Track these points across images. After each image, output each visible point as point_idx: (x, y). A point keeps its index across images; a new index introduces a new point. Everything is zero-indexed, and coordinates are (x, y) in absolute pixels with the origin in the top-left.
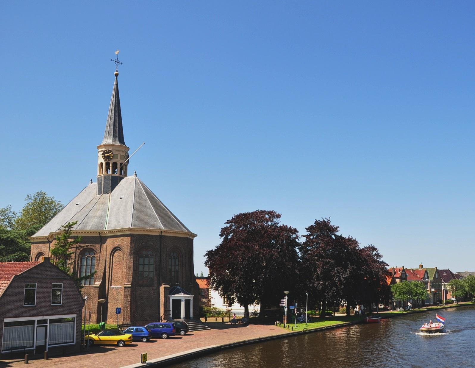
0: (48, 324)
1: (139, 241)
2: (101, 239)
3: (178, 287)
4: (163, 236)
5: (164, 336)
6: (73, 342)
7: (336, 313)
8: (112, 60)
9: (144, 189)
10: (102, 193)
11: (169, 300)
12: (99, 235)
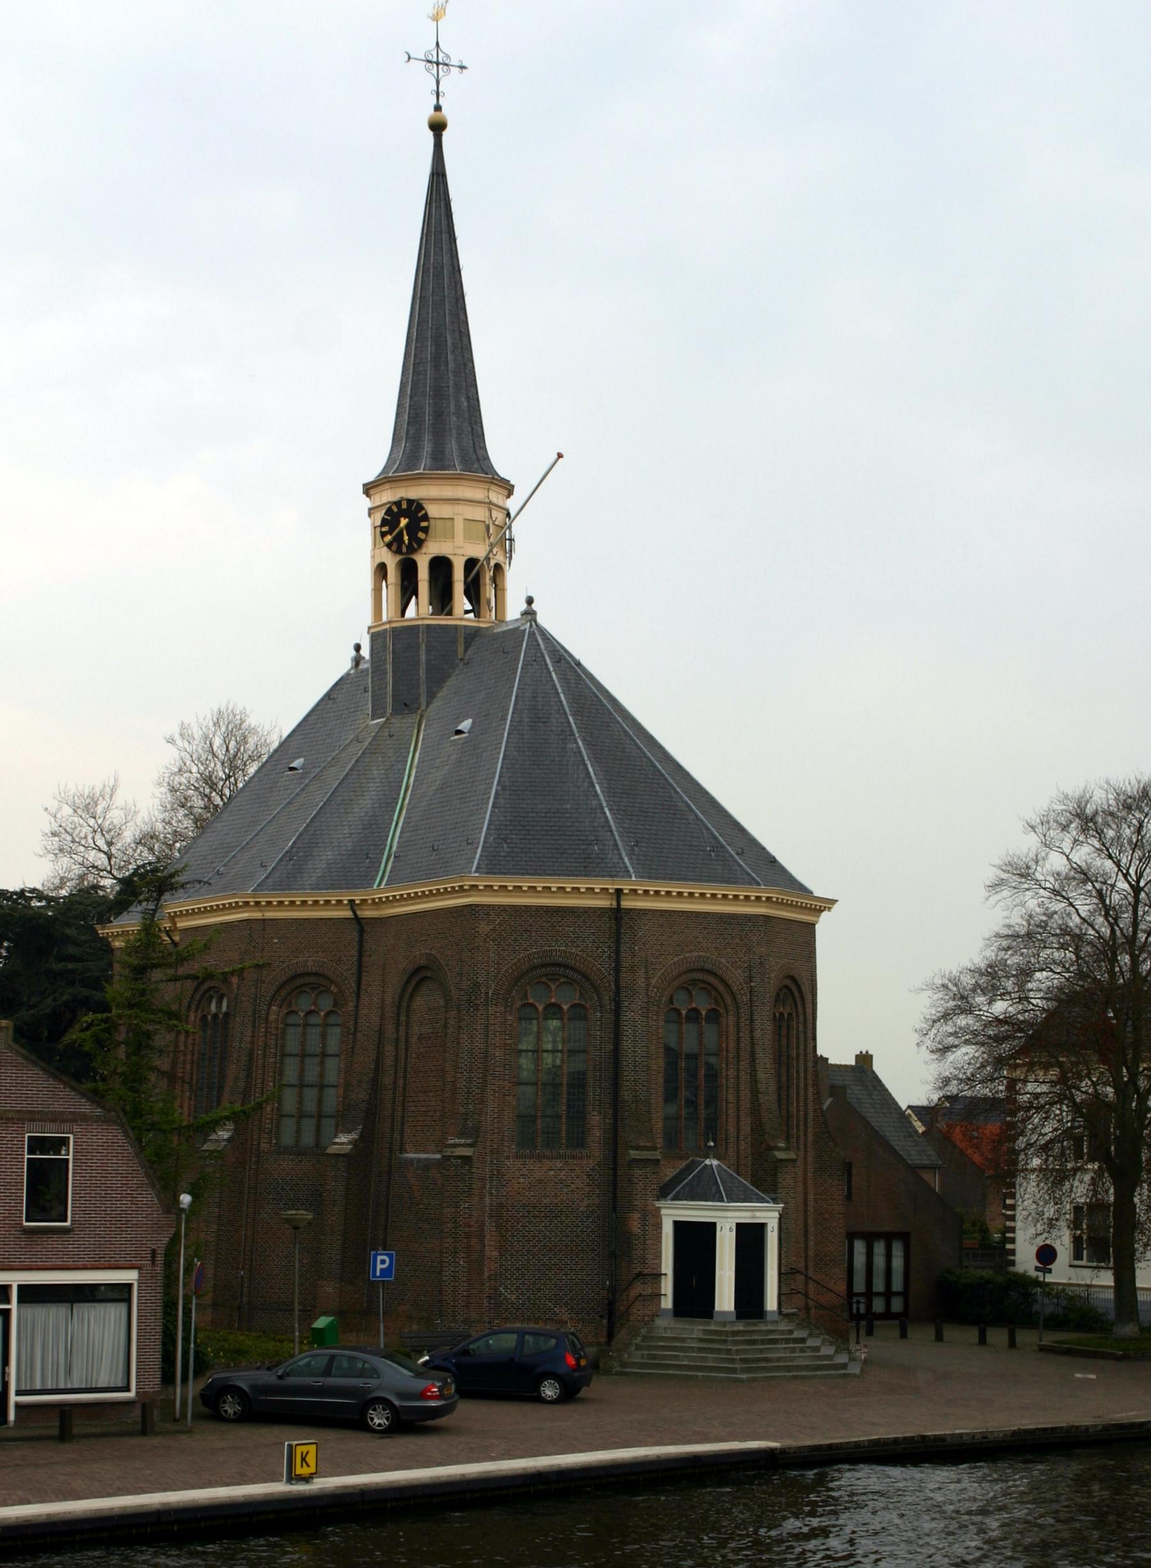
0: (14, 1306)
1: (516, 940)
2: (361, 932)
3: (708, 1162)
4: (630, 911)
5: (549, 1391)
6: (127, 1389)
7: (973, 1334)
8: (409, 58)
9: (564, 679)
10: (389, 711)
11: (659, 1226)
12: (348, 914)
